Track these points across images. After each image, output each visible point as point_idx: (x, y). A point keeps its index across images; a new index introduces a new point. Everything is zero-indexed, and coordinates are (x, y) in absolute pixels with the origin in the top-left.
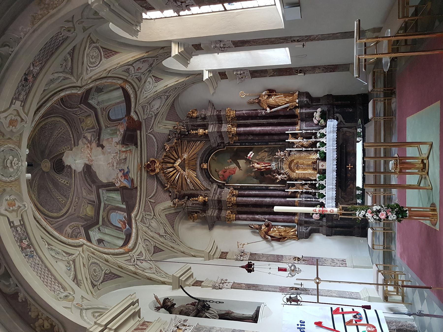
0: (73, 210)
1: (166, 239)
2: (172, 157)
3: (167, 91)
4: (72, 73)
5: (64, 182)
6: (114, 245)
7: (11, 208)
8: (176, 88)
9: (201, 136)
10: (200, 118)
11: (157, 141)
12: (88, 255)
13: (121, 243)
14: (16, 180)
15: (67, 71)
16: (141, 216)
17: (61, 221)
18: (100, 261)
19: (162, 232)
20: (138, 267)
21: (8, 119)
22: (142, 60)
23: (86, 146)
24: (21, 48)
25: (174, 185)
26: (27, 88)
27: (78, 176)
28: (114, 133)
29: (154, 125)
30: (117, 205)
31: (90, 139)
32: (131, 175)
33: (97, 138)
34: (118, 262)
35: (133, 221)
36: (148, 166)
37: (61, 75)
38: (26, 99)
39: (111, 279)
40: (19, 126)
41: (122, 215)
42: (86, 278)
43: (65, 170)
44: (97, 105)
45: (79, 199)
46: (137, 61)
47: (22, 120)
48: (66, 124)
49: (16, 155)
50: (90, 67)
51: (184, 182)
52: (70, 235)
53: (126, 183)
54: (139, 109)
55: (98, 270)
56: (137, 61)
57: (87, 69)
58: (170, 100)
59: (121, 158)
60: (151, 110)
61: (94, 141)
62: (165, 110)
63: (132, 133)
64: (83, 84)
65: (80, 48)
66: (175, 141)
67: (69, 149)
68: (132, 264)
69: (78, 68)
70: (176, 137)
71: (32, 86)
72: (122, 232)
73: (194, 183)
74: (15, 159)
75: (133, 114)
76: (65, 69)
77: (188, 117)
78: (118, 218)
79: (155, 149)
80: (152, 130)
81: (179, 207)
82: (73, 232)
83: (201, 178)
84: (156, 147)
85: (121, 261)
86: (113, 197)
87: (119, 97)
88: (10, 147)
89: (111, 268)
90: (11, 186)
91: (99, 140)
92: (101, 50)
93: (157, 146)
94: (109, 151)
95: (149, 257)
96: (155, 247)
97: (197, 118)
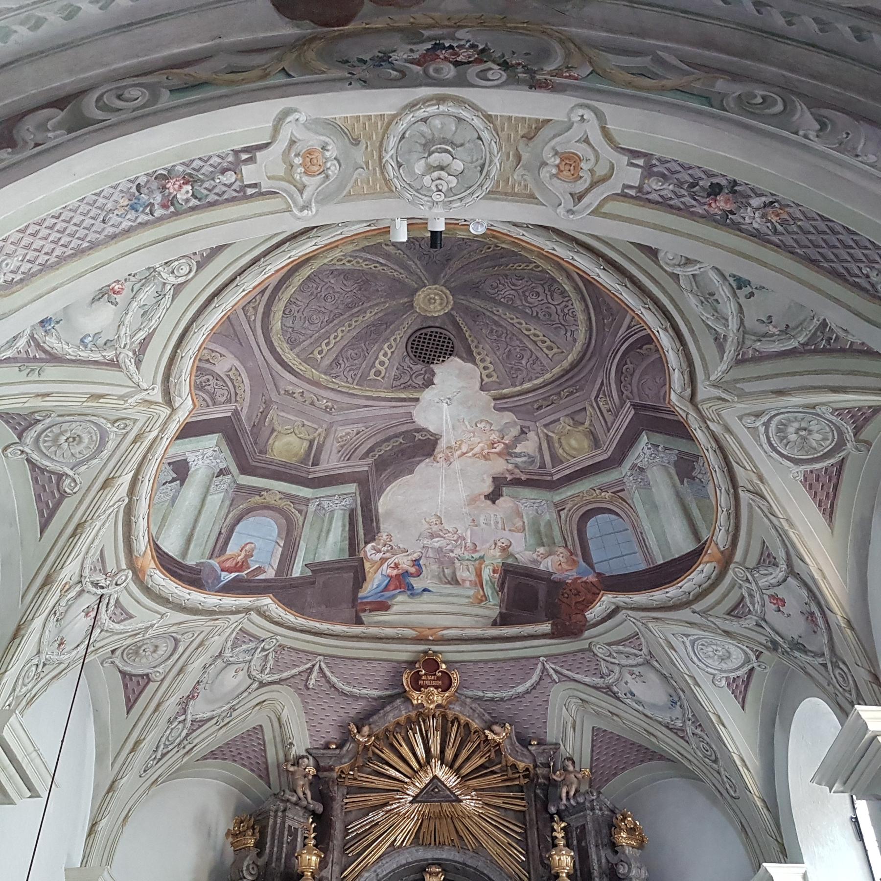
0: (290, 388)
1: (170, 722)
2: (464, 755)
3: (701, 725)
4: (740, 361)
5: (382, 363)
6: (164, 519)
7: (298, 161)
8: (715, 761)
9: (548, 867)
10: (613, 859)
11: (518, 696)
12: (135, 421)
13: (171, 546)
14: (387, 182)
15: (748, 343)
16: (263, 635)
17: (256, 341)
18: (108, 460)
19: (198, 709)
20: (73, 594)
21: (581, 150)
22: (814, 608)
23: (494, 437)
24: (825, 156)
25: (367, 758)
26: (688, 200)
27: (402, 410)
28: (541, 537)
29: (573, 685)
30: (303, 545)
31: (517, 450)
32: (401, 603)
33: (524, 477)
34: (98, 524)
35: (245, 601)
36: (432, 664)
37: (733, 324)
38: (649, 201)
39: (38, 497)
40: (561, 188)
41: (266, 561)
42: (48, 395)
43: (419, 367)
44: (634, 466)
45: (327, 410)
46: (810, 590)
47: (578, 198)
48: (566, 364)
49: (466, 185)
50: (767, 425)
51: (375, 799)
52: (207, 366)
53: (374, 582)
54: (626, 623)
55: (76, 450)
56: (810, 590)
57: (758, 415)
58: (668, 743)
59: (457, 563)
60: (625, 672)
61: (510, 467)
62: (629, 723)
63: (541, 604)
64: (704, 407)
65: (837, 371)
66: (521, 766)
67: (486, 380)
68: (87, 572)
69: (759, 378)
70: (535, 766)
71: (693, 216)
72: (207, 553)
73: (371, 838)
74: (453, 181)
75: (607, 600)
76: (754, 334)
77: (612, 811)
78: (259, 544)
79: (490, 689)
80: (555, 677)
81: (284, 779)
82: (218, 377)
83: (390, 865)
84: (498, 695)
85: (103, 534)
86: (329, 531)
87: (664, 543)
88: (491, 161)
89: (79, 496)
90: (367, 163)
91: (517, 482)
92: (832, 461)
93: (502, 700)
94: (482, 520)
95: (104, 642)
96: (147, 678)
97: (614, 846)
